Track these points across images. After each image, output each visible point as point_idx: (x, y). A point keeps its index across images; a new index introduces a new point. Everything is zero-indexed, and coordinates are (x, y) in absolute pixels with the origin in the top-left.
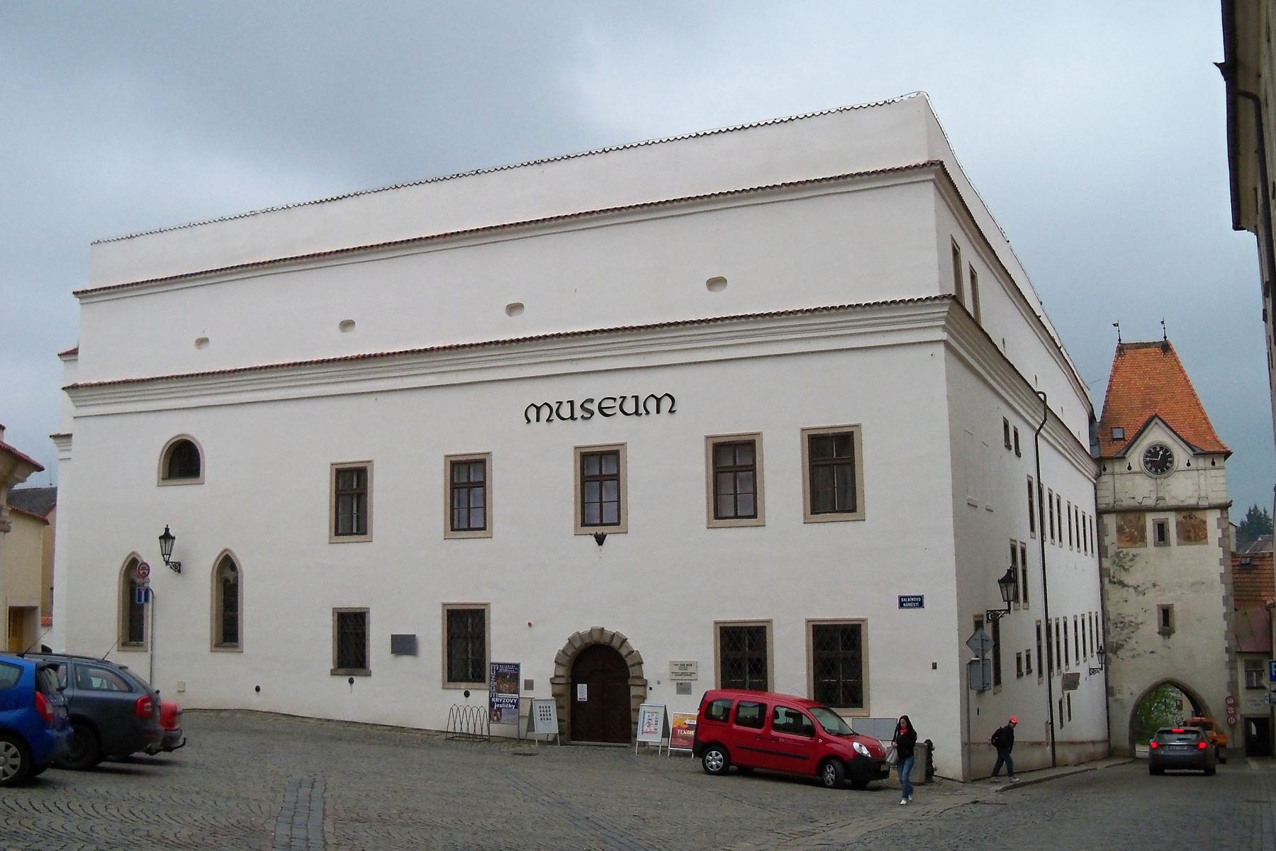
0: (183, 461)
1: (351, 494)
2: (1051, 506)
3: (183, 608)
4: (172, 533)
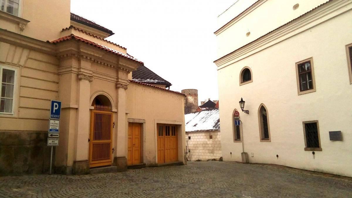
0: (246, 75)
1: (305, 76)
3: (251, 125)
4: (244, 100)
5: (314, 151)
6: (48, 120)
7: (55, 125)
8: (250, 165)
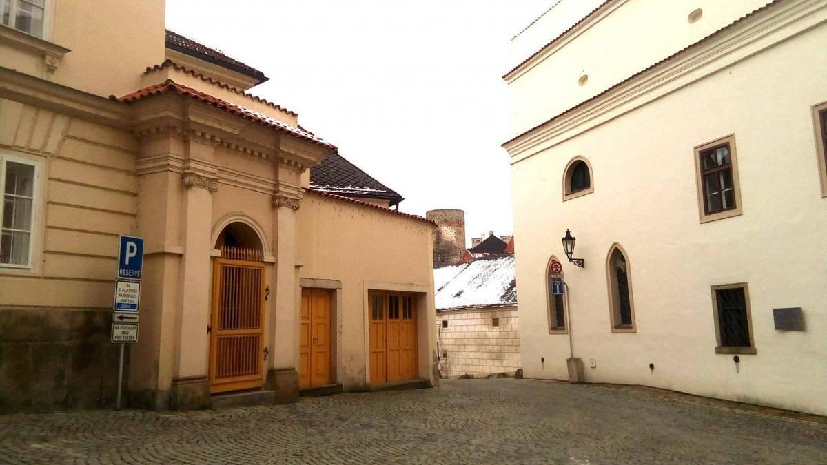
0: (578, 177)
1: (717, 179)
2: (546, 136)
3: (590, 294)
4: (572, 235)
5: (738, 355)
6: (113, 282)
7: (130, 293)
8: (588, 387)
